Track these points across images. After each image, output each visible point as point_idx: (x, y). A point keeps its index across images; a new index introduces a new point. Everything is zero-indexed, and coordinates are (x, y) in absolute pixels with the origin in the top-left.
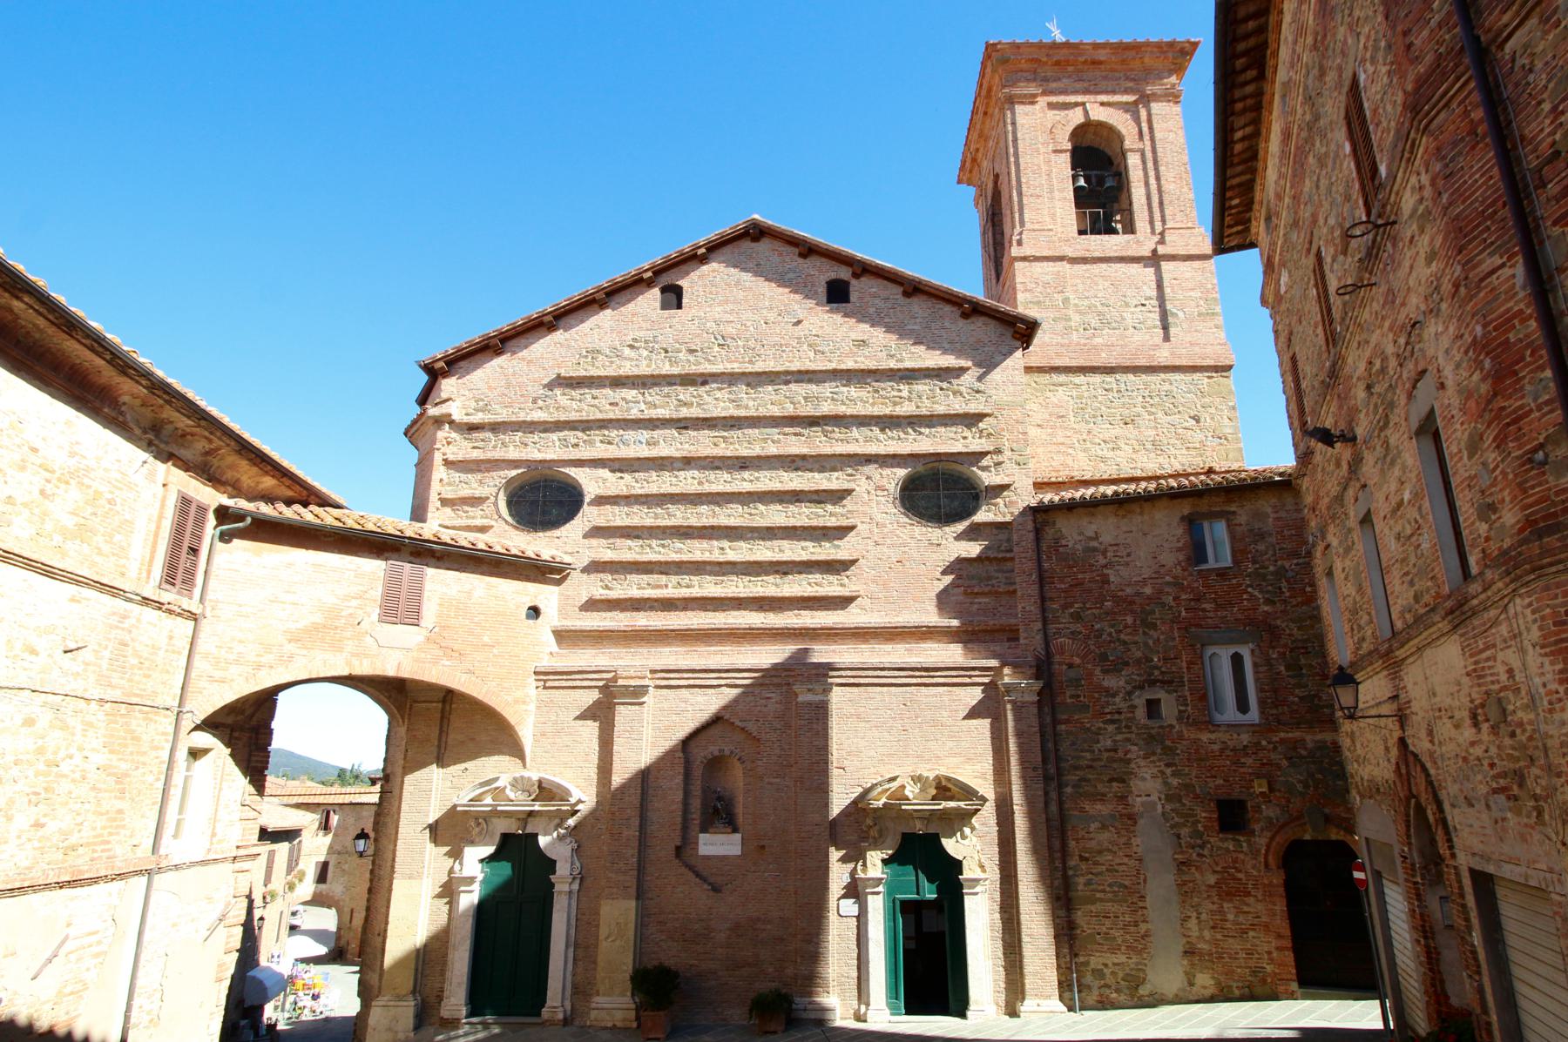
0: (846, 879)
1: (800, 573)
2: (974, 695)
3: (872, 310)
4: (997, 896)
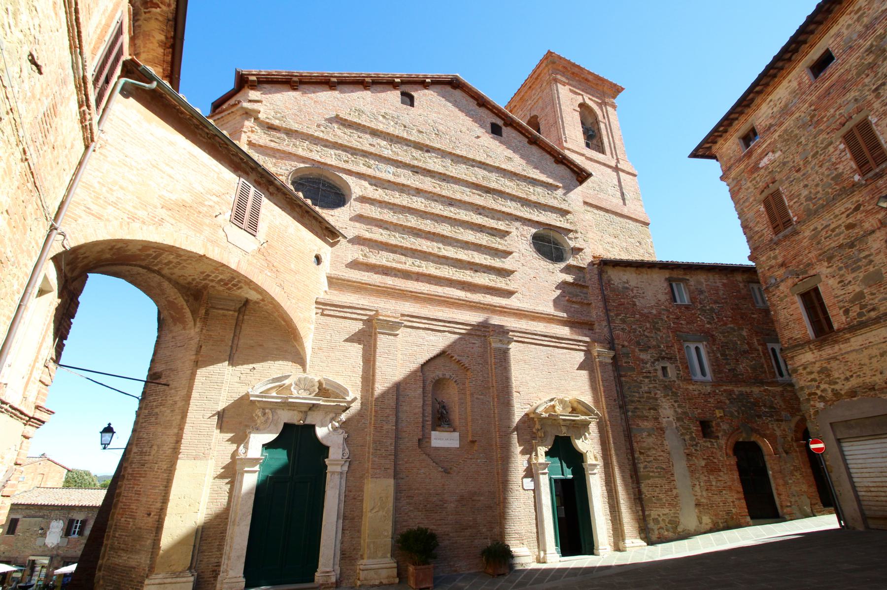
0: (526, 465)
1: (484, 272)
2: (580, 357)
3: (514, 145)
4: (603, 475)
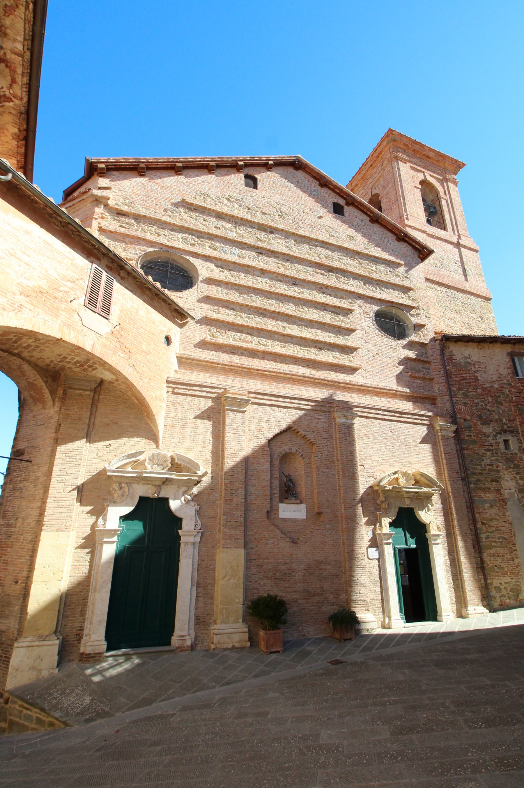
0: (370, 535)
1: (328, 350)
